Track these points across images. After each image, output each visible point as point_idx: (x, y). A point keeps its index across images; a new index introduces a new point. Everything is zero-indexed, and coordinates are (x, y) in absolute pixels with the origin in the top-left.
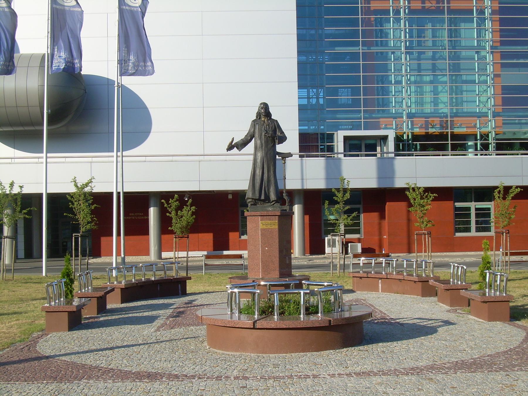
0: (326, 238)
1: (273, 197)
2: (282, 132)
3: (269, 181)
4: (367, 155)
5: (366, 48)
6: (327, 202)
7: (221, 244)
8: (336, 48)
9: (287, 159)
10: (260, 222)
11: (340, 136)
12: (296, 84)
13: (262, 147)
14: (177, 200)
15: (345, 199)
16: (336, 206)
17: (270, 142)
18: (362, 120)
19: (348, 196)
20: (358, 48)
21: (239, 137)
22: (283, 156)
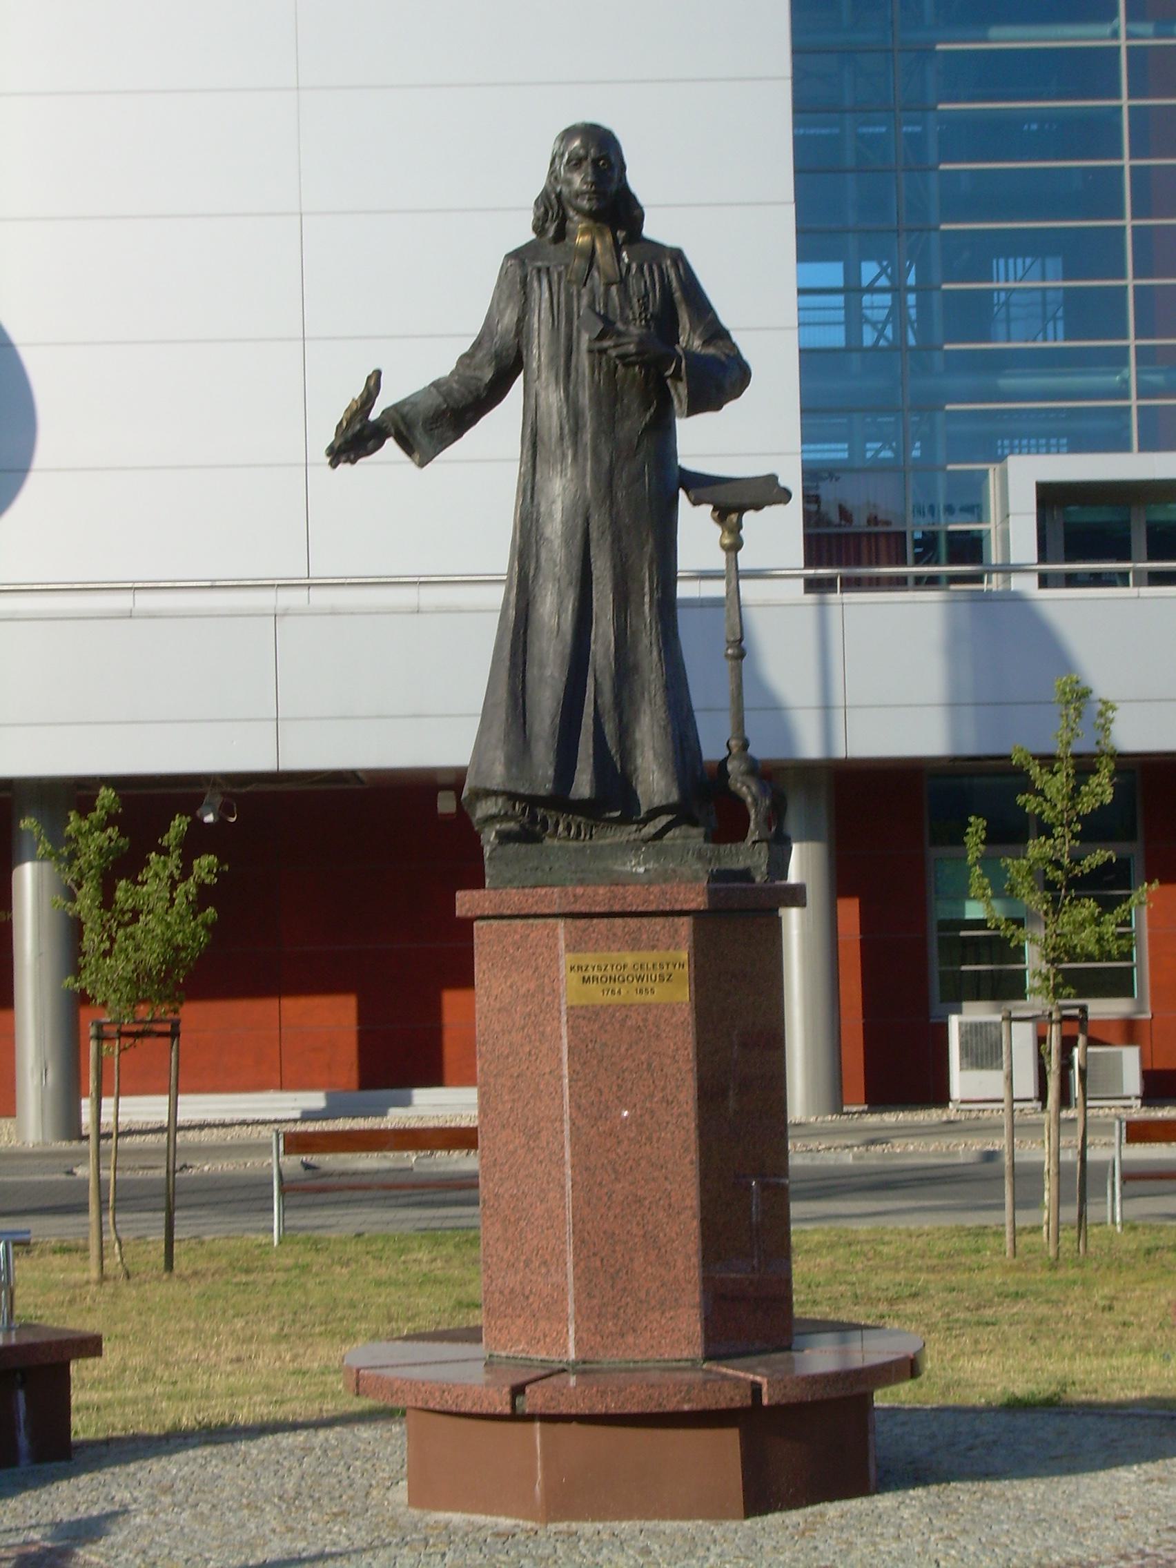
0: (954, 1022)
1: (654, 781)
2: (718, 334)
3: (625, 670)
4: (1158, 579)
5: (1148, 28)
6: (977, 826)
7: (403, 1050)
8: (994, 32)
9: (749, 517)
10: (566, 960)
11: (1014, 491)
12: (786, 217)
13: (576, 431)
14: (111, 820)
15: (1086, 805)
16: (1036, 848)
17: (631, 400)
18: (1134, 403)
19: (1101, 789)
20: (1106, 29)
21: (418, 367)
22: (730, 499)
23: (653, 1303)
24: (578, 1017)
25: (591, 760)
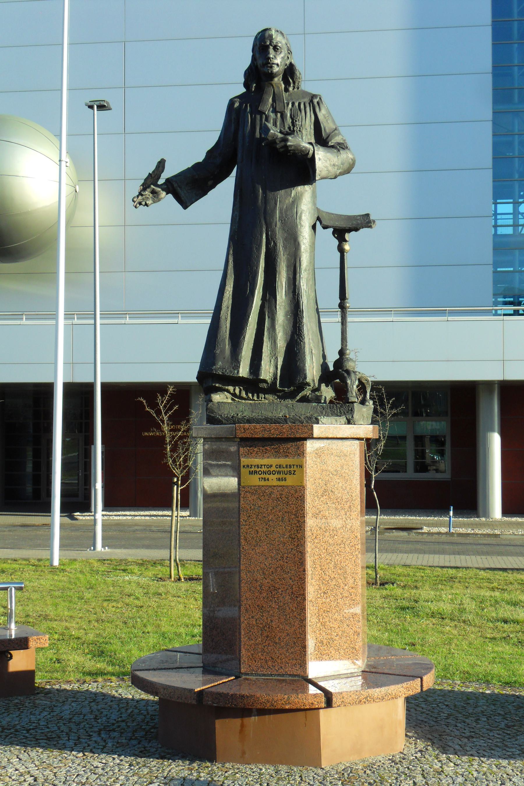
23: (282, 644)
24: (246, 492)
25: (285, 349)
